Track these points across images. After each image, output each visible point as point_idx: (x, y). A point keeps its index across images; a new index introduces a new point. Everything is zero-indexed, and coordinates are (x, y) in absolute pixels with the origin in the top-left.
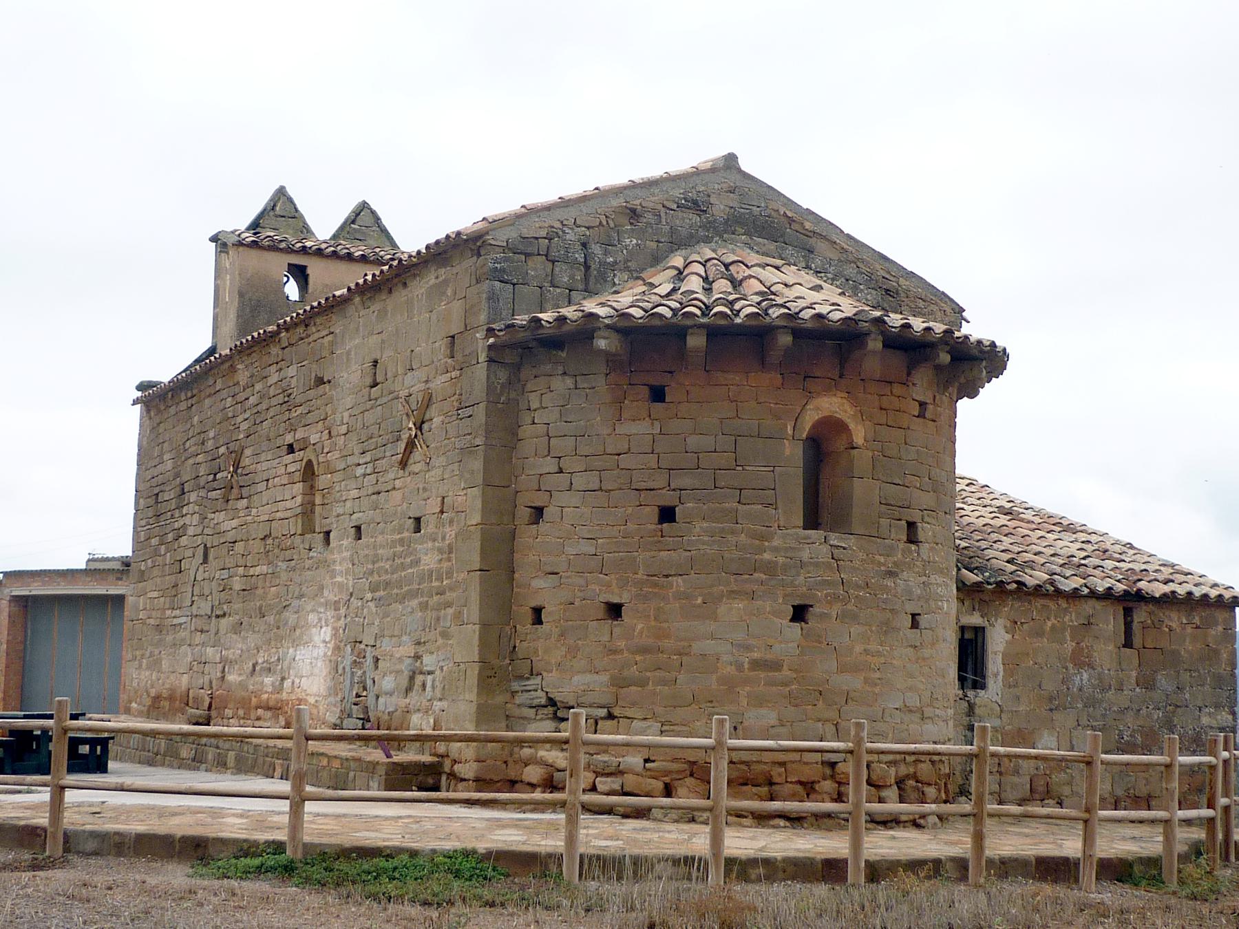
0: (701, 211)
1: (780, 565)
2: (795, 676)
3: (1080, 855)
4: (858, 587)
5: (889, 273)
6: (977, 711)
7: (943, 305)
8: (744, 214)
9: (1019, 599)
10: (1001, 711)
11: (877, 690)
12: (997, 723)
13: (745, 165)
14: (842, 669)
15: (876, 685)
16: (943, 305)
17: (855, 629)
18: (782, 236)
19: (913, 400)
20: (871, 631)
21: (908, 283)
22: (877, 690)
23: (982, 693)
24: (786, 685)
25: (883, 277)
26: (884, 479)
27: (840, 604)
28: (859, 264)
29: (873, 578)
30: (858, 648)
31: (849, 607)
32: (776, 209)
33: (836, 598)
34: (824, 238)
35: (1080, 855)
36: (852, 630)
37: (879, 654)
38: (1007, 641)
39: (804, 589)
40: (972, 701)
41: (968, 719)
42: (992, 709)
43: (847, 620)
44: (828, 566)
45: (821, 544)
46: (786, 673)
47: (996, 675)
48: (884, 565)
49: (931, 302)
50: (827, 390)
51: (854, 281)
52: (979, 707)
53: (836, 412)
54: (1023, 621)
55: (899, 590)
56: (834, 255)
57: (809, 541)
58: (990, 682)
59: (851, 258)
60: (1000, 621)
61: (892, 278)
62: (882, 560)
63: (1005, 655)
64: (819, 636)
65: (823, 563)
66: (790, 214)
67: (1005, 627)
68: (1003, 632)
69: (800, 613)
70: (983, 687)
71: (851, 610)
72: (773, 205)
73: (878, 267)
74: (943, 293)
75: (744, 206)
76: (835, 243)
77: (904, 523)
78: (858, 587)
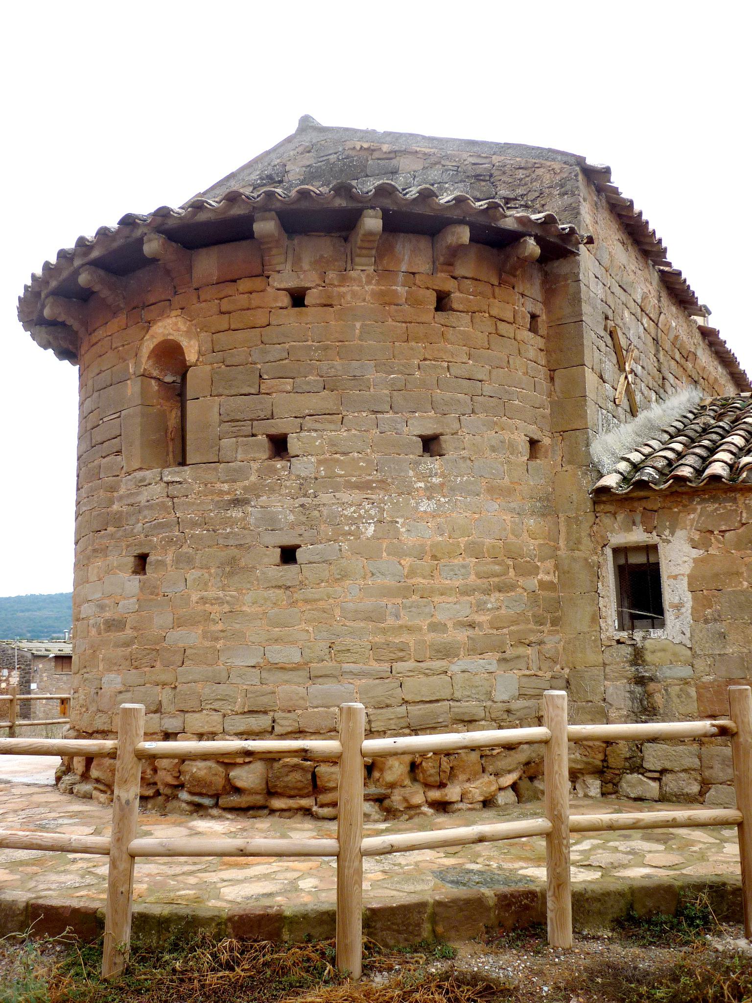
0: (276, 182)
1: (124, 514)
2: (136, 635)
3: (335, 908)
4: (194, 524)
5: (479, 156)
6: (649, 657)
7: (549, 163)
8: (320, 167)
9: (714, 499)
10: (695, 656)
11: (219, 645)
12: (685, 672)
13: (325, 121)
14: (179, 623)
15: (217, 639)
16: (549, 163)
17: (193, 575)
18: (362, 171)
19: (278, 289)
20: (210, 575)
21: (503, 158)
22: (219, 645)
23: (656, 633)
24: (128, 646)
25: (474, 164)
26: (227, 392)
27: (174, 548)
28: (443, 162)
29: (211, 511)
30: (194, 598)
31: (185, 549)
32: (352, 147)
33: (170, 541)
34: (405, 152)
35: (335, 908)
36: (188, 576)
37: (219, 601)
38: (694, 559)
39: (142, 536)
40: (640, 645)
41: (633, 669)
42: (675, 654)
43: (181, 566)
44: (163, 506)
45: (156, 483)
46: (129, 632)
47: (678, 607)
48: (228, 493)
49: (534, 167)
50: (162, 314)
51: (439, 183)
52: (653, 652)
53: (170, 334)
54: (723, 528)
55: (252, 520)
56: (418, 166)
57: (145, 483)
58: (669, 616)
59: (433, 159)
60: (681, 534)
61: (484, 161)
62: (226, 487)
63: (692, 579)
64: (154, 587)
65: (157, 504)
66: (365, 145)
67: (692, 540)
68: (687, 548)
69: (142, 562)
70: (662, 625)
71: (186, 553)
72: (349, 145)
73: (465, 155)
74: (550, 150)
75: (321, 159)
76: (416, 152)
77: (262, 438)
78: (194, 524)
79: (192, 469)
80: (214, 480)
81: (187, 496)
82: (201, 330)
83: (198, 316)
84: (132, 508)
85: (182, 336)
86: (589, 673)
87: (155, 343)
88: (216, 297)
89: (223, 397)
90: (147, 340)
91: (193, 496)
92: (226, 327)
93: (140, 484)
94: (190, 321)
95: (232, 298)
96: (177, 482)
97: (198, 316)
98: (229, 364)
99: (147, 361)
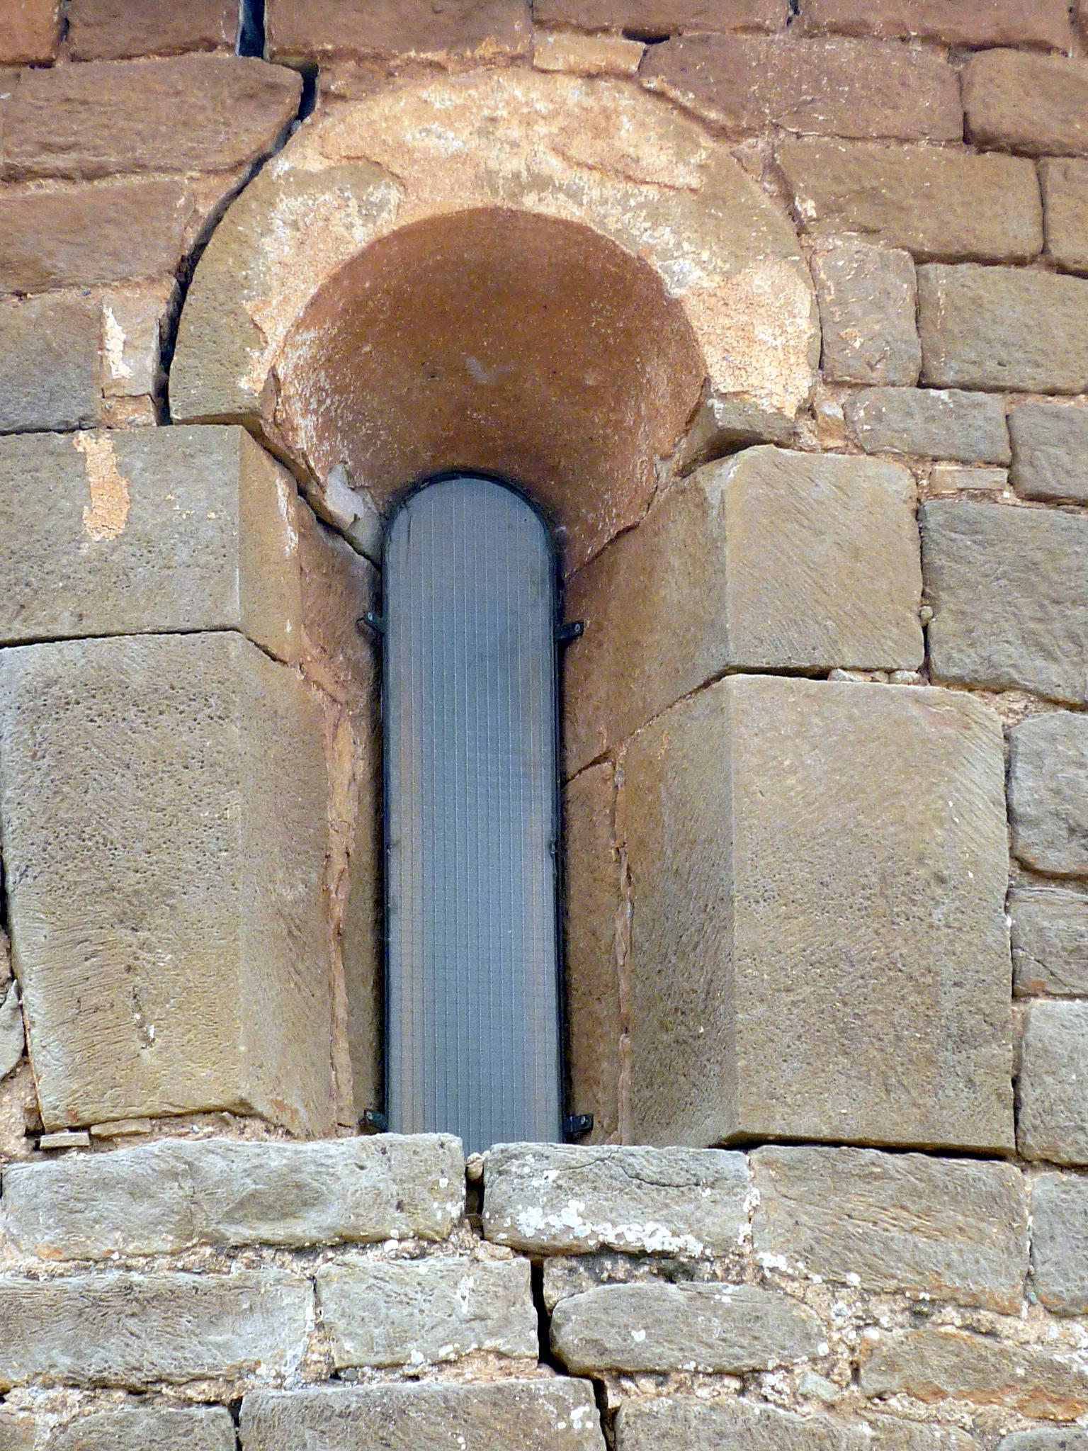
53: (541, 183)
57: (304, 1228)
79: (791, 1174)
80: (1003, 1287)
81: (748, 1378)
82: (827, 209)
83: (799, 112)
84: (145, 1418)
85: (656, 215)
86: (87, 1214)
87: (388, 223)
88: (933, 24)
89: (1016, 701)
90: (302, 182)
91: (814, 1383)
92: (1025, 237)
93: (236, 1233)
94: (720, 133)
95: (1042, 60)
96: (637, 1257)
97: (799, 112)
98: (1051, 483)
99: (299, 325)
